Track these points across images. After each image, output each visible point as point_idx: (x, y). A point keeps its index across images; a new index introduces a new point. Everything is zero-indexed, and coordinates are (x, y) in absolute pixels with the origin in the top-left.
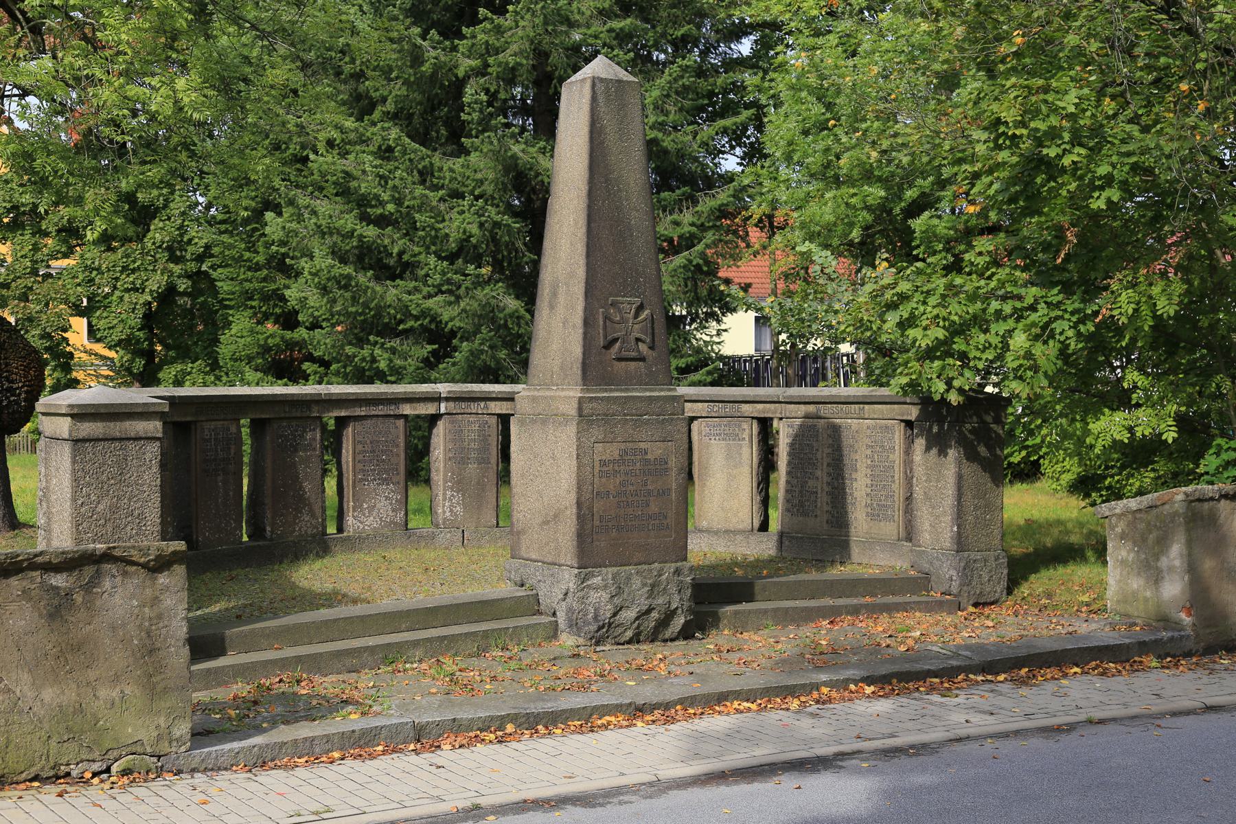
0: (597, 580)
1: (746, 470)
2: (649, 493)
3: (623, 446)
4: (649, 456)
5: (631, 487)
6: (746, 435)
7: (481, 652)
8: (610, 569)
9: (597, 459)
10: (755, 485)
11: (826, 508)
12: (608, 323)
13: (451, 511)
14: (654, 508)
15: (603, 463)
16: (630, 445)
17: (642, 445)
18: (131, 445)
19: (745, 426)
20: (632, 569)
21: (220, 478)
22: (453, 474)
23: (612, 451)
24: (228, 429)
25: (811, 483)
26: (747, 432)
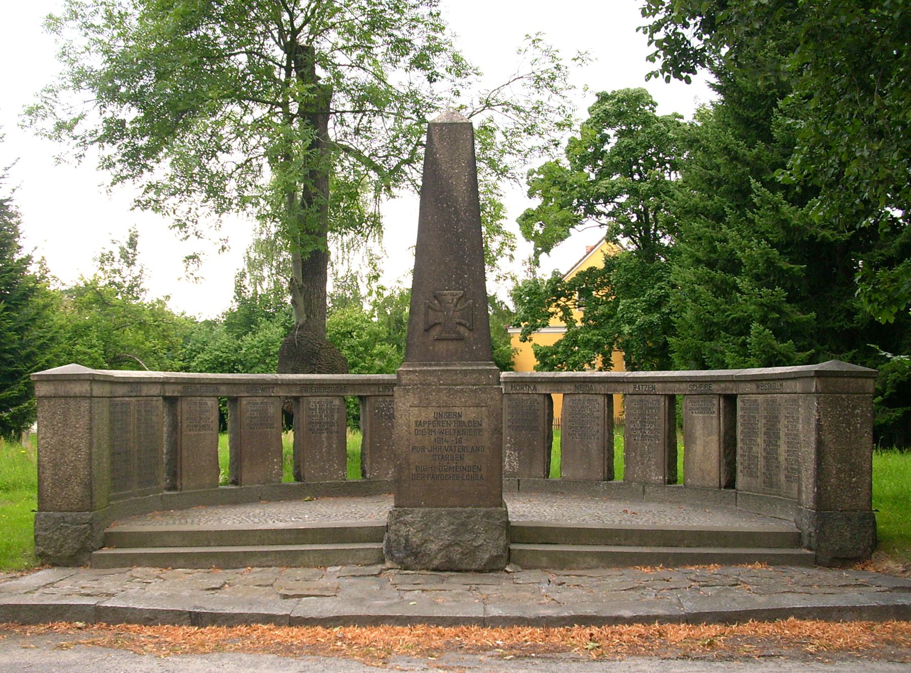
0: (408, 518)
1: (715, 438)
2: (464, 449)
3: (438, 410)
4: (463, 419)
5: (445, 444)
6: (715, 409)
7: (324, 565)
8: (422, 510)
9: (413, 419)
10: (722, 450)
11: (763, 471)
12: (430, 311)
13: (510, 465)
14: (468, 461)
15: (418, 423)
16: (445, 410)
17: (457, 410)
18: (72, 402)
19: (715, 402)
20: (443, 511)
21: (325, 435)
22: (511, 438)
23: (429, 414)
24: (332, 402)
25: (754, 449)
26: (716, 406)
